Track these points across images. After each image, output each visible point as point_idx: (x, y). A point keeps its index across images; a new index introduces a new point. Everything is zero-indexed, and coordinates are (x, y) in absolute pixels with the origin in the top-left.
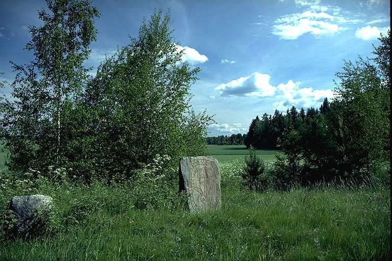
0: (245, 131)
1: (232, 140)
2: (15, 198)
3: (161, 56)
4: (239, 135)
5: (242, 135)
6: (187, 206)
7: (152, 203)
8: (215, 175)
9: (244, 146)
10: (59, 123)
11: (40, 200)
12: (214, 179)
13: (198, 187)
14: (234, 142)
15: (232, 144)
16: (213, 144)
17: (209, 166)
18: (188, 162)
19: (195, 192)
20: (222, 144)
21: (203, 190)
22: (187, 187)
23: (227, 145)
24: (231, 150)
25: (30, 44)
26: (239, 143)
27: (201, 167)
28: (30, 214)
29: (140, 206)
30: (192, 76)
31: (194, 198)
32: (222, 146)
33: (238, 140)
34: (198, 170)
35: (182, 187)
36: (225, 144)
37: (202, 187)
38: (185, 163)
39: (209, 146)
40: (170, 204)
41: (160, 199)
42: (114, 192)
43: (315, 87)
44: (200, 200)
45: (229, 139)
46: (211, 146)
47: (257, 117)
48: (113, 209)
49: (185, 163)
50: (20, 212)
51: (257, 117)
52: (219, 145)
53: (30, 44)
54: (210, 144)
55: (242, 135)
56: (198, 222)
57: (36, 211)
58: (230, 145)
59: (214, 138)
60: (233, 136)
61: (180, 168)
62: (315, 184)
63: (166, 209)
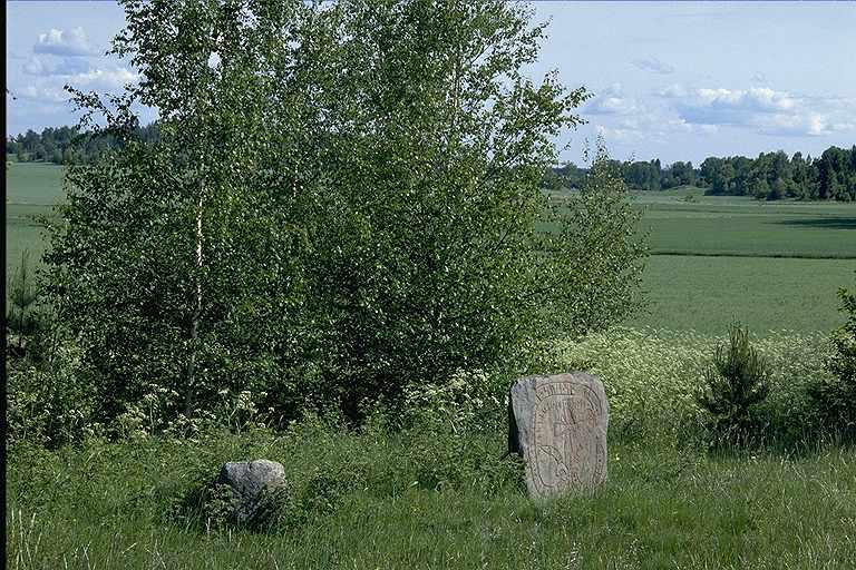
1: (824, 179)
2: (229, 465)
3: (477, 50)
6: (521, 485)
7: (451, 478)
10: (199, 251)
11: (269, 469)
14: (835, 186)
15: (822, 197)
16: (731, 193)
17: (579, 397)
18: (529, 390)
19: (544, 456)
20: (774, 196)
21: (562, 451)
22: (525, 445)
23: (802, 198)
24: (800, 232)
25: (123, 39)
27: (560, 398)
28: (256, 492)
29: (428, 482)
30: (565, 114)
32: (775, 204)
34: (549, 408)
35: (515, 445)
36: (791, 193)
38: (521, 391)
39: (712, 201)
41: (465, 470)
43: (671, 341)
45: (810, 171)
46: (725, 201)
49: (521, 391)
52: (760, 196)
53: (123, 39)
54: (717, 190)
56: (533, 515)
57: (265, 488)
58: (812, 198)
59: (738, 162)
61: (510, 403)
63: (477, 489)
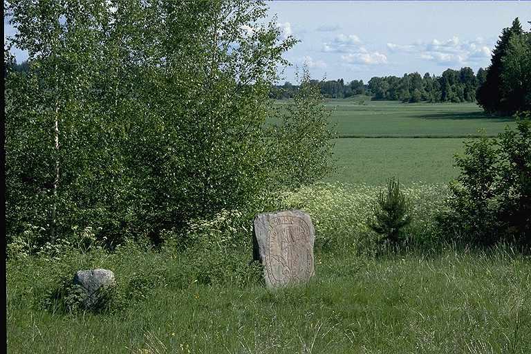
0: (481, 60)
1: (443, 88)
4: (466, 73)
5: (475, 74)
8: (304, 237)
9: (474, 106)
10: (57, 140)
11: (105, 275)
12: (303, 243)
13: (279, 254)
14: (451, 94)
15: (443, 100)
16: (387, 99)
17: (296, 225)
18: (265, 222)
19: (275, 262)
20: (413, 100)
23: (431, 101)
26: (465, 97)
27: (284, 226)
31: (273, 269)
33: (462, 88)
34: (277, 233)
35: (257, 256)
36: (424, 99)
37: (285, 255)
40: (239, 278)
41: (227, 273)
42: (165, 260)
44: (281, 273)
47: (516, 23)
48: (177, 283)
50: (87, 286)
51: (516, 23)
52: (405, 101)
54: (379, 97)
55: (475, 74)
56: (268, 299)
57: (102, 286)
58: (436, 101)
60: (448, 76)
61: (254, 229)
62: (497, 244)
